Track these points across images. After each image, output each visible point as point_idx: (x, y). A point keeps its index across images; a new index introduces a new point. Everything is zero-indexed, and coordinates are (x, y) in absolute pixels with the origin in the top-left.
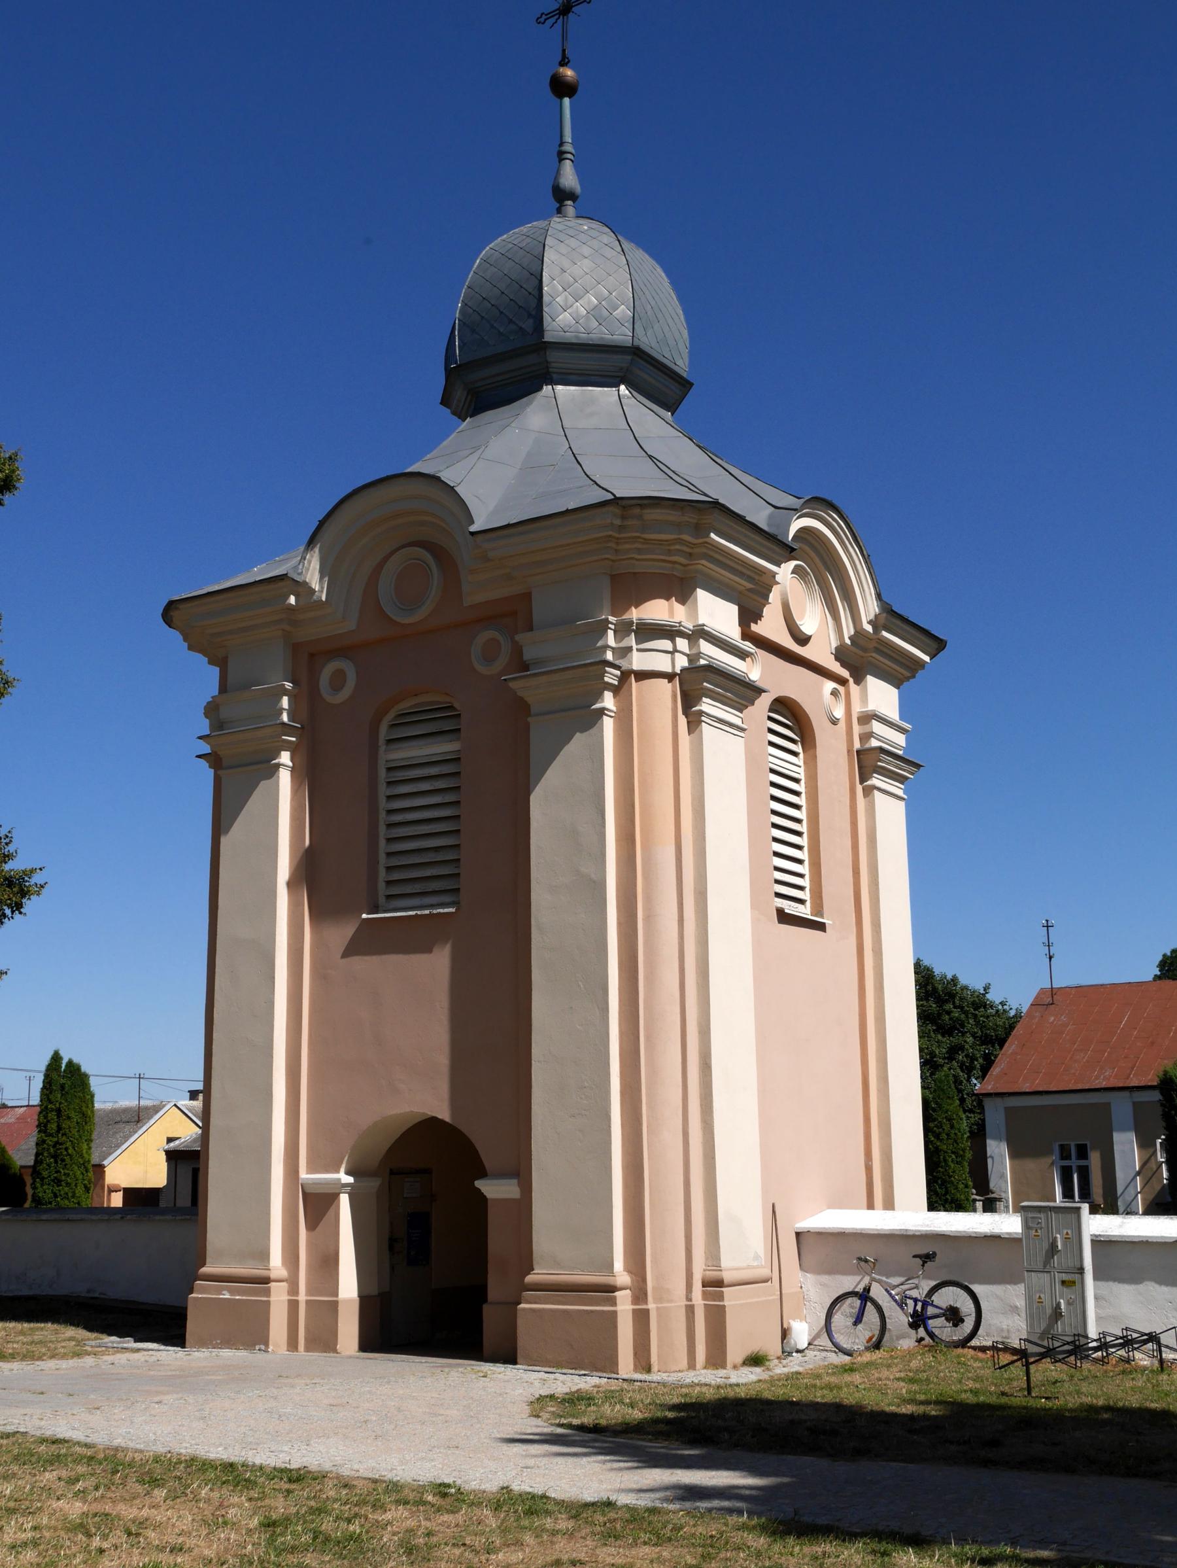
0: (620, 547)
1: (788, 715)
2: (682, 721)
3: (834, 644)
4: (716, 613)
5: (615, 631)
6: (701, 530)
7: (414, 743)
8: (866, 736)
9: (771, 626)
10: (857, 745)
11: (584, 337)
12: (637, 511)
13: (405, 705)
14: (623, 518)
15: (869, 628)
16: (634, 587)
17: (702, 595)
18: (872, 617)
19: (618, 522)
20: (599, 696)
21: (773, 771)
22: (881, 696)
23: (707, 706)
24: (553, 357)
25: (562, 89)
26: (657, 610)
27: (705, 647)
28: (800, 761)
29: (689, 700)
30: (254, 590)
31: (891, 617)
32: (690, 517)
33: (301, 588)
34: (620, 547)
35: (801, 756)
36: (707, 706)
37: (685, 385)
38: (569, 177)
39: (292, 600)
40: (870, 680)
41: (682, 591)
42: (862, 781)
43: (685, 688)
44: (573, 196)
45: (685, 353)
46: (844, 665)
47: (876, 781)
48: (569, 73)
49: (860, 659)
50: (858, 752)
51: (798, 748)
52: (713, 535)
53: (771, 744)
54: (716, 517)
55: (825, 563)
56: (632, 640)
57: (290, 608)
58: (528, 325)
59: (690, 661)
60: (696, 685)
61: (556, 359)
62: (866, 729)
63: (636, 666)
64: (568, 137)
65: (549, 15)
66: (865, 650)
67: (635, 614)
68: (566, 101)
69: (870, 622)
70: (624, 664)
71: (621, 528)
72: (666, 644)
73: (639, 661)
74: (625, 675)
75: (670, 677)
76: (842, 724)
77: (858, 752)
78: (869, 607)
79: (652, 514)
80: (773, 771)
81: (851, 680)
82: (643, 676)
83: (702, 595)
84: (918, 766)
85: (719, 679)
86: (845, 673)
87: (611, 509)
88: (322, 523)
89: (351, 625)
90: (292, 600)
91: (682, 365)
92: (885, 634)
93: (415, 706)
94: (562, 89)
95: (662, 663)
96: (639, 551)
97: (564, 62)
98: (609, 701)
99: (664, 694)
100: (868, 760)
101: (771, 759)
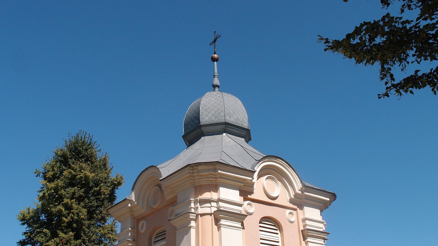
0: (195, 178)
1: (273, 222)
2: (215, 227)
3: (289, 198)
4: (233, 195)
5: (194, 203)
6: (216, 170)
7: (159, 242)
8: (305, 226)
9: (258, 194)
10: (302, 228)
11: (212, 122)
12: (195, 167)
13: (157, 231)
14: (193, 170)
15: (300, 192)
16: (200, 189)
17: (221, 189)
18: (300, 188)
19: (192, 171)
20: (190, 223)
21: (261, 239)
22: (312, 213)
23: (223, 222)
24: (203, 129)
25: (214, 60)
26: (207, 195)
27: (221, 204)
28: (279, 235)
29: (217, 221)
30: (122, 203)
31: (305, 188)
32: (210, 167)
33: (130, 201)
34: (195, 178)
35: (279, 234)
36: (223, 222)
37: (248, 131)
38: (216, 81)
39: (129, 205)
40: (305, 208)
41: (215, 188)
42: (304, 239)
43: (216, 217)
44: (218, 87)
45: (247, 121)
46: (294, 204)
47: (309, 239)
48: (216, 56)
49: (299, 202)
50: (302, 231)
51: (278, 232)
52: (219, 171)
53: (260, 230)
54: (218, 166)
55: (281, 175)
56: (198, 205)
57: (130, 207)
58: (197, 122)
59: (218, 209)
60: (218, 217)
61: (204, 129)
62: (304, 223)
63: (199, 213)
64: (216, 72)
65: (212, 43)
66: (302, 199)
67: (200, 197)
68: (215, 62)
69: (299, 190)
70: (197, 212)
71: (193, 173)
72: (208, 205)
73: (201, 211)
74: (197, 215)
75: (211, 214)
76: (296, 223)
77: (302, 231)
78: (298, 185)
79: (200, 168)
80: (261, 239)
81: (298, 209)
82: (202, 215)
83: (221, 189)
84: (328, 233)
85: (226, 213)
86: (295, 207)
87: (188, 168)
88: (135, 183)
89: (144, 210)
90: (129, 205)
91: (246, 125)
92: (305, 193)
93: (160, 231)
94: (214, 60)
95: (208, 211)
96: (200, 179)
97: (215, 53)
98: (193, 224)
99: (210, 220)
100: (305, 233)
101: (261, 235)
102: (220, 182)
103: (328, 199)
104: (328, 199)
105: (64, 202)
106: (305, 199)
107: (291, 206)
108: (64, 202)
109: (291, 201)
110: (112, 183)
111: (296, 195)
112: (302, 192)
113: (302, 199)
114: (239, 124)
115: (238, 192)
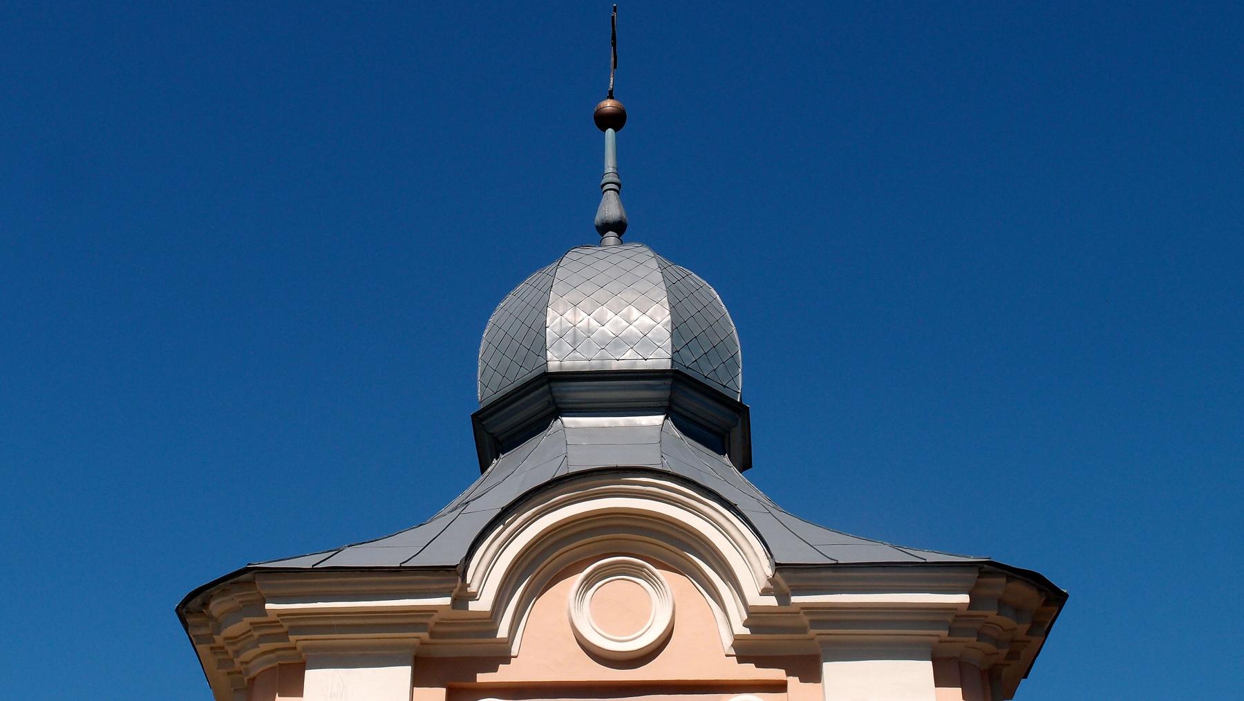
3: (728, 641)
15: (772, 601)
18: (764, 583)
25: (604, 120)
66: (803, 630)
69: (765, 592)
81: (793, 682)
86: (777, 674)
92: (794, 599)
94: (604, 120)
102: (306, 649)
103: (964, 598)
104: (964, 598)
105: (221, 657)
106: (815, 624)
107: (750, 672)
108: (221, 657)
109: (744, 651)
110: (553, 402)
111: (755, 618)
112: (783, 598)
113: (803, 630)
114: (627, 359)
115: (929, 664)
